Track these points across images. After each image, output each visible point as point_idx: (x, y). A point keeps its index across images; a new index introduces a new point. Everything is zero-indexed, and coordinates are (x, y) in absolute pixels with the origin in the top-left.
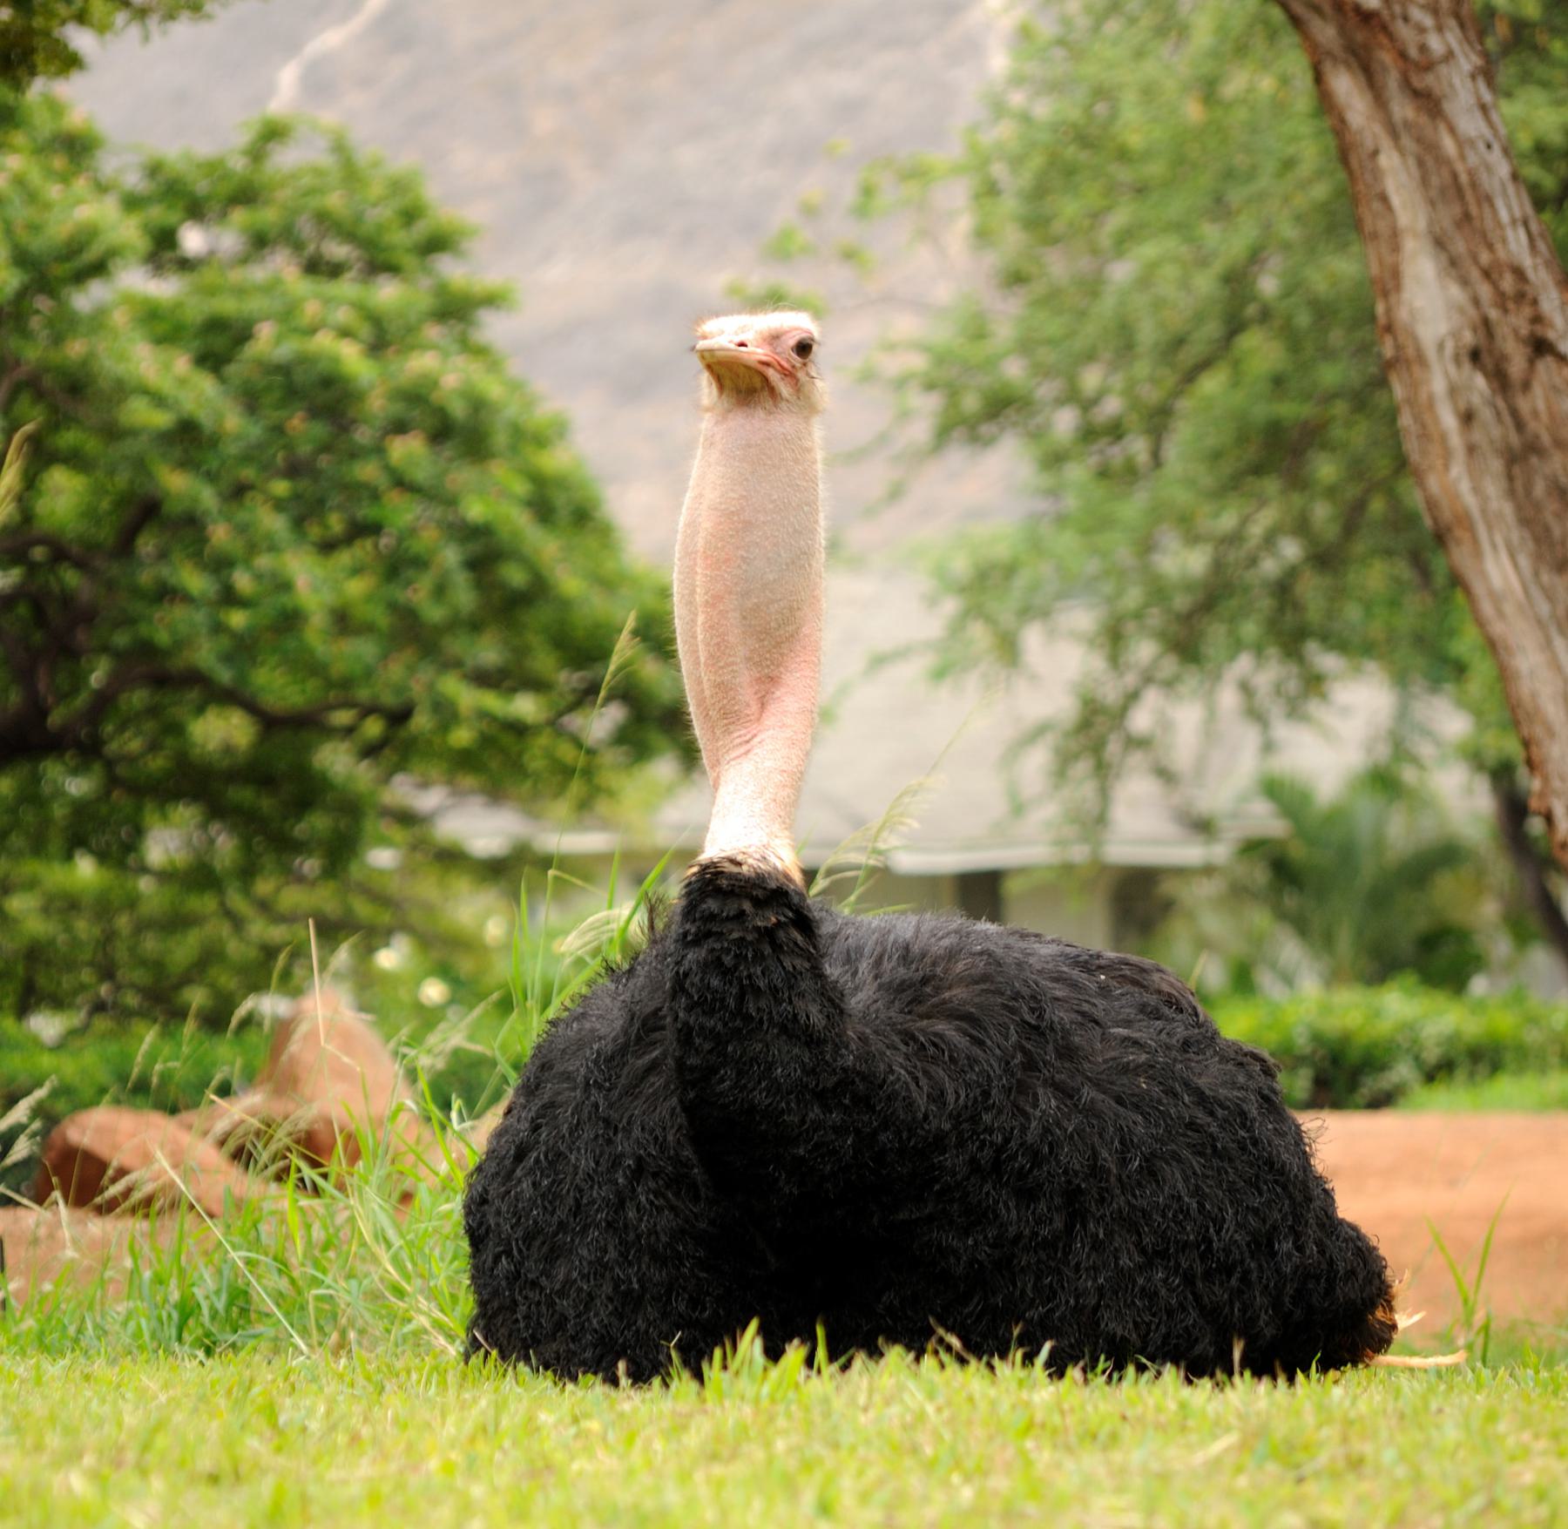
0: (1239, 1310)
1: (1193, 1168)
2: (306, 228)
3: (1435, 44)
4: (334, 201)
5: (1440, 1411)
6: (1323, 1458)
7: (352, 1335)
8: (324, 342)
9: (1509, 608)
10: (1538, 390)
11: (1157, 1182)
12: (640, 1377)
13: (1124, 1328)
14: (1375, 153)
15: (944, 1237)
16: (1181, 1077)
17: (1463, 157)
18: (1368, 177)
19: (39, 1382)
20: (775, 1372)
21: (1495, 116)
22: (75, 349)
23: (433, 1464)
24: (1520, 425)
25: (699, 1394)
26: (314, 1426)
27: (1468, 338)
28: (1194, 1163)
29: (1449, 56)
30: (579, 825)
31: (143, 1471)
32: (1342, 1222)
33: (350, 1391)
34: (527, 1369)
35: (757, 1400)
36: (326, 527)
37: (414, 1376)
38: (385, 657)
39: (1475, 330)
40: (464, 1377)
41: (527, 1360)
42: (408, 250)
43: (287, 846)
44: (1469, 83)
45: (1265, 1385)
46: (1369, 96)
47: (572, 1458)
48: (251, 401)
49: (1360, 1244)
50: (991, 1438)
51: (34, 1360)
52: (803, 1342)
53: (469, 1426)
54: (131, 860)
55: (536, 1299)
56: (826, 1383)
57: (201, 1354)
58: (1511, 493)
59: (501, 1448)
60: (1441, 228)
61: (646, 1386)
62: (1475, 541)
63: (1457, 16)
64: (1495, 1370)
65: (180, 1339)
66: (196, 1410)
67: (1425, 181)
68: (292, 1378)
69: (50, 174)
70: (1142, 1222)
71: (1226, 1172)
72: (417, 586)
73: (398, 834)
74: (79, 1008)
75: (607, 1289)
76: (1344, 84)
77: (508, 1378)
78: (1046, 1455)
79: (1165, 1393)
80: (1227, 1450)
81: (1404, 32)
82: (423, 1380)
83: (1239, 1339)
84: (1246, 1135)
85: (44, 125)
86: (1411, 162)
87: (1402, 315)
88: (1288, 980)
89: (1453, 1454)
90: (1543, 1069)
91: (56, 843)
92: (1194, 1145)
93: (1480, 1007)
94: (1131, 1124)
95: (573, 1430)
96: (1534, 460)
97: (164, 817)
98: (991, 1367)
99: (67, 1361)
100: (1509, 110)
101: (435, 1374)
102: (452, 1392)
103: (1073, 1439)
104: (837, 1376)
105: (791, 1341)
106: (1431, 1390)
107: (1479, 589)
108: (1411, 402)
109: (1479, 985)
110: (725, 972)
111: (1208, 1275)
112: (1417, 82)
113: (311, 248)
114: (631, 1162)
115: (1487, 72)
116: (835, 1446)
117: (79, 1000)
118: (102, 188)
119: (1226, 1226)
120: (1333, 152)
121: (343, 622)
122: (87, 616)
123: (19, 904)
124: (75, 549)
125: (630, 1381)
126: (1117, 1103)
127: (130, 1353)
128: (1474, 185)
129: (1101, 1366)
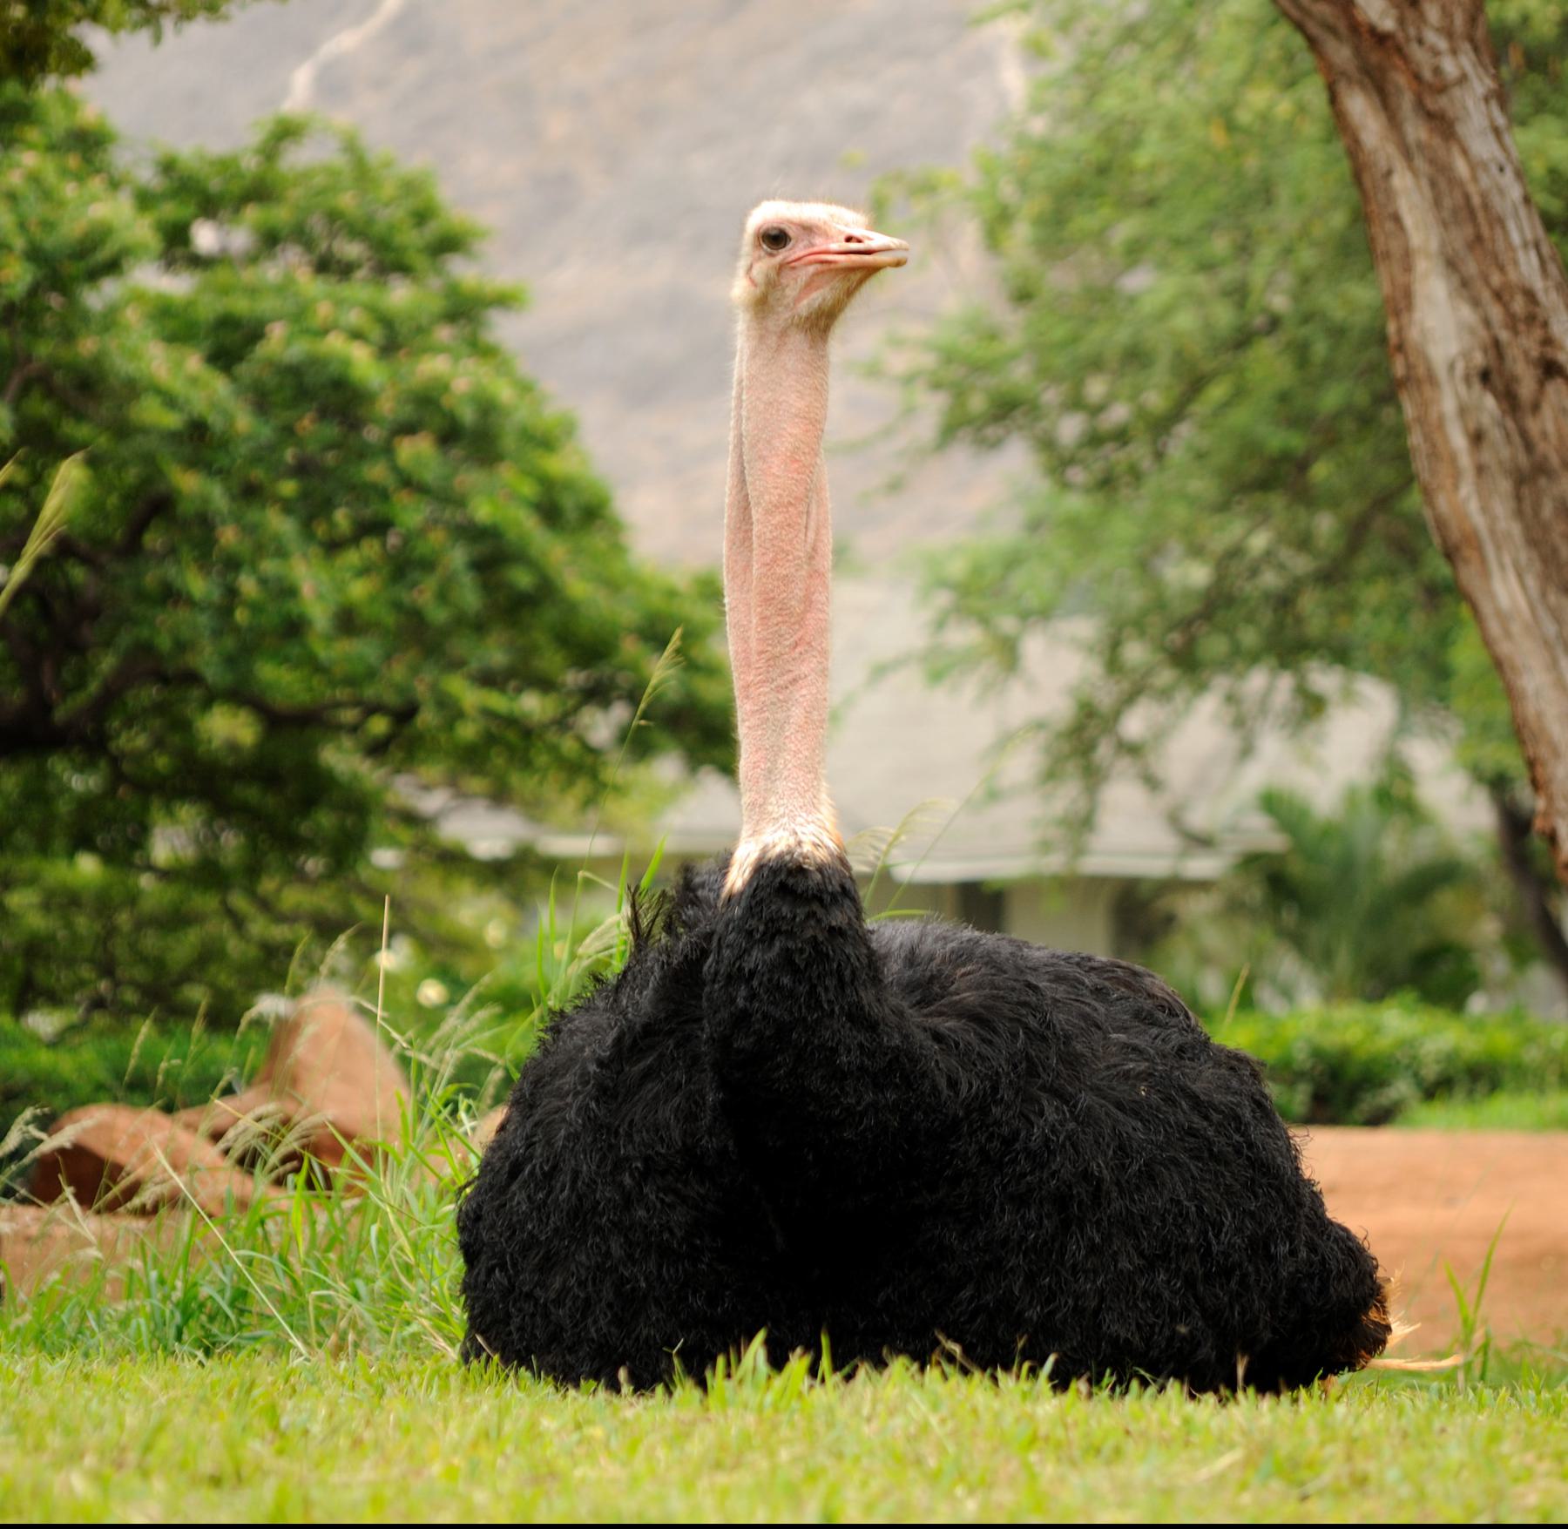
0: (1239, 1314)
1: (1189, 1170)
2: (317, 224)
3: (1450, 67)
4: (347, 201)
5: (1443, 1430)
6: (1327, 1476)
7: (351, 1337)
8: (335, 343)
9: (1516, 628)
10: (1547, 412)
11: (1156, 1186)
12: (642, 1384)
13: (1128, 1330)
14: (1389, 173)
15: (947, 1235)
16: (1179, 1085)
17: (1475, 179)
18: (1381, 197)
19: (37, 1382)
20: (779, 1381)
21: (1508, 139)
22: (87, 346)
23: (436, 1469)
24: (1529, 446)
25: (701, 1401)
26: (316, 1429)
27: (1479, 359)
28: (1192, 1167)
29: (1463, 79)
30: (580, 830)
31: (145, 1473)
32: (1331, 1223)
33: (351, 1394)
34: (528, 1374)
35: (761, 1409)
36: (332, 524)
37: (416, 1380)
38: (388, 657)
39: (1485, 351)
40: (466, 1380)
41: (530, 1367)
42: (420, 251)
43: (292, 844)
44: (1482, 106)
45: (1268, 1402)
46: (1382, 117)
47: (575, 1465)
48: (262, 401)
49: (1350, 1244)
50: (995, 1450)
51: (33, 1358)
52: (806, 1350)
53: (471, 1431)
54: (137, 858)
55: (531, 1311)
56: (830, 1392)
57: (200, 1354)
58: (1519, 513)
59: (504, 1455)
60: (1453, 250)
61: (648, 1393)
62: (1483, 561)
63: (1471, 39)
64: (1496, 1389)
65: (179, 1338)
66: (196, 1411)
67: (1437, 203)
68: (292, 1380)
69: (64, 173)
70: (1141, 1225)
71: (1223, 1176)
72: (422, 586)
73: (406, 835)
74: (78, 1004)
75: (608, 1294)
76: (1359, 105)
77: (509, 1384)
78: (1050, 1469)
79: (1169, 1407)
80: (1231, 1466)
81: (1418, 54)
82: (424, 1384)
83: (1243, 1356)
84: (1241, 1139)
85: (58, 120)
86: (1424, 183)
87: (1413, 334)
88: (1287, 993)
89: (1457, 1474)
90: (1541, 1088)
91: (59, 843)
92: (1191, 1150)
93: (1478, 1026)
94: (1130, 1130)
95: (575, 1437)
96: (1543, 482)
97: (170, 813)
98: (994, 1379)
99: (66, 1360)
100: (1522, 139)
101: (436, 1378)
102: (453, 1395)
103: (1077, 1453)
104: (841, 1385)
105: (793, 1350)
106: (1433, 1409)
107: (1487, 609)
108: (1421, 420)
109: (1477, 1004)
110: (795, 971)
111: (1208, 1277)
112: (1431, 103)
113: (323, 246)
114: (639, 1165)
115: (1500, 96)
116: (839, 1456)
117: (77, 997)
118: (114, 185)
119: (1224, 1230)
120: (1348, 177)
121: (348, 622)
122: (92, 613)
123: (20, 900)
124: (83, 545)
125: (632, 1388)
126: (1118, 1108)
127: (129, 1352)
128: (1486, 206)
129: (1106, 1380)
